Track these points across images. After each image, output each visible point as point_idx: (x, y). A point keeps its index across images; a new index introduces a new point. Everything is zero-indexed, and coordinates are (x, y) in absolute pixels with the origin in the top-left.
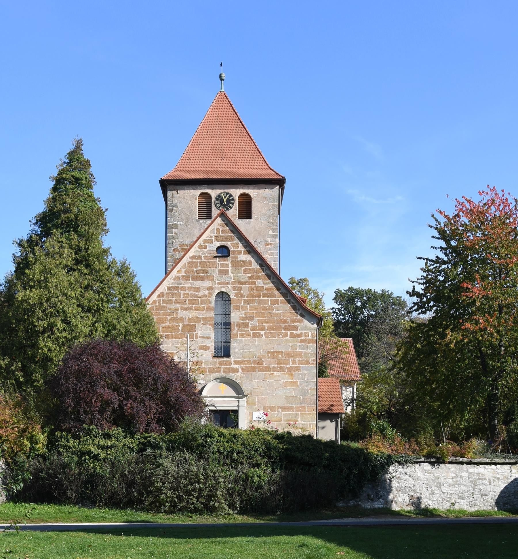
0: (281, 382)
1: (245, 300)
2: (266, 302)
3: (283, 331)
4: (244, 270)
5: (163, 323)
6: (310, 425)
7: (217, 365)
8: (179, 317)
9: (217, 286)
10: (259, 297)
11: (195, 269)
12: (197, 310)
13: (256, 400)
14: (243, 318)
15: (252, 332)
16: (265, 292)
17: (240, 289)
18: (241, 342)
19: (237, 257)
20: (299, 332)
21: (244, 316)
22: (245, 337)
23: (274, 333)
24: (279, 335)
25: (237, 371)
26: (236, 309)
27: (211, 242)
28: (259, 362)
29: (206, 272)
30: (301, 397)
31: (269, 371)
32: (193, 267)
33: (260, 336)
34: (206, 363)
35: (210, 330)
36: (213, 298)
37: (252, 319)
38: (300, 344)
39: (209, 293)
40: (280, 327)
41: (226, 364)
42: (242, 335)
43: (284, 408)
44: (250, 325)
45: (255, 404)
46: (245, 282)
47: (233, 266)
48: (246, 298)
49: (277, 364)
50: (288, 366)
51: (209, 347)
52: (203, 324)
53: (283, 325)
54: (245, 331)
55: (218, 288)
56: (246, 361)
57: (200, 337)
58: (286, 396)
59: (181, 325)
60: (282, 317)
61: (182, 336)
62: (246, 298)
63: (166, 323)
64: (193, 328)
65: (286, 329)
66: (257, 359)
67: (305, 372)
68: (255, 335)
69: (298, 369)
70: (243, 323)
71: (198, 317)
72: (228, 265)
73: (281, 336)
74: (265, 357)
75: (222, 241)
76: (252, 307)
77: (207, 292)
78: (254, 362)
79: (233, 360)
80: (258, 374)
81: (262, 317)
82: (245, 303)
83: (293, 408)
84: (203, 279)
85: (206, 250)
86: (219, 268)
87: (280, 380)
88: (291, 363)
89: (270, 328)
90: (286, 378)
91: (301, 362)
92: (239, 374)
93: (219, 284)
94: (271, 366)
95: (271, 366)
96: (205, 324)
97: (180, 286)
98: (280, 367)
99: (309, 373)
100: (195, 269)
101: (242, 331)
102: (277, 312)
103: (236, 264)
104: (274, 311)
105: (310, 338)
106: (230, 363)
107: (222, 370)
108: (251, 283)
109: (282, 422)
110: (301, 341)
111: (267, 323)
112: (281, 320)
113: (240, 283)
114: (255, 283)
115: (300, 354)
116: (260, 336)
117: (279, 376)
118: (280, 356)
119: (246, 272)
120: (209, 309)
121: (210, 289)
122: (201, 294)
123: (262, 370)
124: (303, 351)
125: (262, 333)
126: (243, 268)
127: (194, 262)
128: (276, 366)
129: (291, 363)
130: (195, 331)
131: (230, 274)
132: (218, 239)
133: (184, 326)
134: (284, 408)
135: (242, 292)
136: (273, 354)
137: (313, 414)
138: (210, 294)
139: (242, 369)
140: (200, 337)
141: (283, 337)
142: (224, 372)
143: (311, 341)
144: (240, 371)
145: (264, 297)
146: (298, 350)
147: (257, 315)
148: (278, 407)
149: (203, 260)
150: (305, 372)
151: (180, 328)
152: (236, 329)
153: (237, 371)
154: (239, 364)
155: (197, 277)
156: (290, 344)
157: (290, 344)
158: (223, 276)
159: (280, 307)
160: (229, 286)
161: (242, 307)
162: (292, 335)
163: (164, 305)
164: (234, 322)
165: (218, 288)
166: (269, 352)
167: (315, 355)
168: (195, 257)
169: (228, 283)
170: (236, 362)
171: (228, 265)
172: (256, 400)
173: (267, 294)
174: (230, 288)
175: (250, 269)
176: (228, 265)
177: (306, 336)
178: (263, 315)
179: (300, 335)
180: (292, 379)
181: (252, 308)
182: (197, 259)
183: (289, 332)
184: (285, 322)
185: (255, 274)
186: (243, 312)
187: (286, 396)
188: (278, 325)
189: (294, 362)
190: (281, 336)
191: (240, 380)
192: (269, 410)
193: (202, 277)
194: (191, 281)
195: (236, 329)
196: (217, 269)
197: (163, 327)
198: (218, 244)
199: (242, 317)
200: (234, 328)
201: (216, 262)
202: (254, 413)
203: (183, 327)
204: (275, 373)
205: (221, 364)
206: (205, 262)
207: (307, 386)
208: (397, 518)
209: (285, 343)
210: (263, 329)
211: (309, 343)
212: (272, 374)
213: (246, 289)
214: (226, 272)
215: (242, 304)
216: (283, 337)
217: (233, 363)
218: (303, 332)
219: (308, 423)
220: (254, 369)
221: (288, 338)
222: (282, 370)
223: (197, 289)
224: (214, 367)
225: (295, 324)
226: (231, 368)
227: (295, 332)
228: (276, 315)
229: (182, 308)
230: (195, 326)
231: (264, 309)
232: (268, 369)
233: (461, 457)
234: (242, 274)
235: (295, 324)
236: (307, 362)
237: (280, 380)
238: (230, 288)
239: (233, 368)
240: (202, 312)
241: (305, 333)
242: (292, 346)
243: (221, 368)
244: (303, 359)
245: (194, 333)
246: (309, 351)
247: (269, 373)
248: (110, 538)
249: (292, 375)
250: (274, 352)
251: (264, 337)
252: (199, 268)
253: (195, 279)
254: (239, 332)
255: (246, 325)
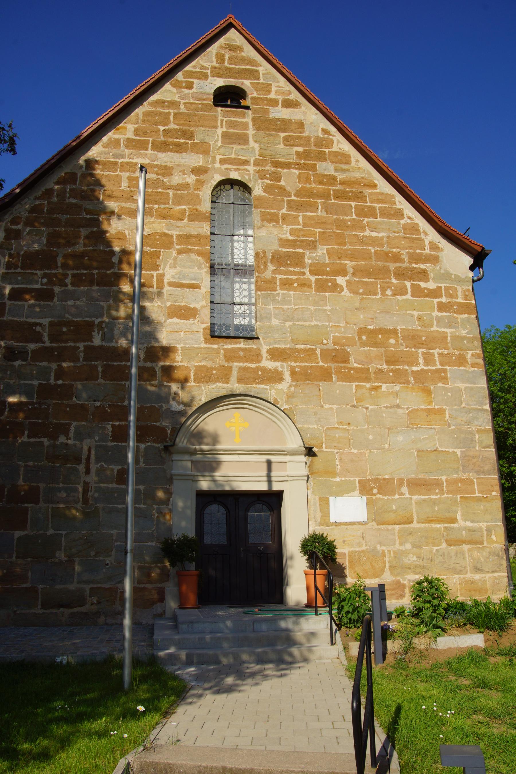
0: (400, 411)
2: (346, 211)
3: (394, 280)
4: (285, 139)
5: (69, 244)
7: (220, 361)
9: (217, 165)
11: (162, 128)
12: (165, 217)
13: (337, 462)
15: (313, 278)
16: (338, 187)
17: (277, 177)
19: (267, 111)
20: (431, 285)
21: (291, 238)
22: (295, 289)
23: (372, 283)
25: (275, 377)
26: (269, 221)
28: (339, 356)
29: (190, 135)
30: (458, 452)
31: (367, 379)
32: (157, 123)
33: (335, 288)
34: (188, 352)
35: (200, 268)
36: (206, 193)
37: (312, 246)
38: (440, 314)
39: (197, 180)
41: (246, 359)
42: (287, 284)
43: (417, 485)
44: (307, 261)
45: (334, 474)
46: (290, 163)
50: (415, 369)
51: (195, 309)
52: (179, 252)
53: (392, 266)
55: (218, 171)
57: (171, 284)
58: (419, 451)
60: (385, 248)
63: (74, 244)
65: (400, 274)
66: (331, 346)
67: (462, 386)
68: (321, 286)
69: (441, 376)
70: (288, 256)
71: (166, 235)
72: (245, 126)
73: (389, 292)
74: (350, 342)
76: (311, 218)
77: (191, 179)
78: (326, 355)
80: (338, 386)
81: (338, 244)
82: (289, 208)
84: (179, 148)
85: (191, 91)
86: (224, 129)
87: (398, 406)
90: (413, 400)
91: (446, 359)
92: (283, 386)
93: (223, 161)
94: (372, 367)
95: (372, 367)
96: (188, 251)
97: (120, 161)
98: (395, 372)
99: (471, 389)
100: (162, 128)
103: (265, 124)
104: (367, 233)
105: (460, 300)
106: (258, 357)
107: (235, 373)
108: (305, 167)
109: (415, 525)
110: (442, 307)
111: (352, 258)
112: (387, 254)
113: (276, 164)
114: (313, 167)
115: (440, 340)
116: (335, 288)
117: (396, 394)
118: (392, 341)
120: (196, 216)
121: (198, 171)
122: (176, 179)
123: (347, 378)
124: (448, 330)
125: (341, 280)
126: (282, 135)
127: (161, 113)
128: (385, 366)
129: (421, 361)
131: (252, 143)
132: (217, 73)
134: (417, 485)
135: (282, 183)
136: (374, 337)
138: (200, 183)
139: (293, 373)
140: (171, 284)
141: (394, 295)
142: (240, 380)
143: (463, 308)
144: (287, 376)
145: (336, 197)
146: (435, 328)
147: (324, 238)
150: (462, 386)
152: (271, 267)
154: (284, 360)
155: (165, 143)
156: (416, 313)
157: (416, 313)
158: (235, 147)
159: (381, 223)
160: (251, 168)
161: (284, 217)
162: (417, 292)
163: (74, 201)
165: (218, 171)
166: (362, 331)
167: (477, 343)
168: (164, 102)
169: (246, 162)
170: (276, 354)
171: (245, 126)
172: (337, 462)
175: (301, 138)
176: (247, 124)
178: (340, 240)
179: (435, 293)
182: (169, 107)
183: (408, 284)
184: (397, 258)
186: (287, 228)
187: (419, 451)
188: (380, 264)
189: (428, 359)
190: (389, 292)
191: (287, 402)
192: (375, 491)
193: (178, 145)
194: (150, 152)
198: (220, 82)
199: (288, 240)
200: (266, 266)
204: (384, 387)
205: (230, 356)
206: (189, 115)
207: (469, 423)
209: (401, 312)
210: (343, 272)
211: (459, 312)
213: (290, 179)
214: (243, 139)
215: (284, 211)
216: (394, 295)
217: (264, 354)
218: (443, 286)
219: (484, 525)
220: (326, 375)
221: (409, 296)
222: (399, 377)
223: (167, 171)
224: (209, 364)
225: (422, 266)
227: (423, 285)
228: (373, 241)
230: (157, 255)
231: (340, 224)
232: (362, 375)
233: (69, 247)
234: (282, 146)
235: (422, 266)
236: (461, 361)
237: (398, 406)
238: (252, 172)
239: (264, 370)
240: (179, 224)
241: (447, 289)
242: (419, 319)
243: (231, 368)
244: (451, 351)
245: (155, 273)
247: (368, 385)
248: (252, 394)
249: (427, 392)
251: (346, 292)
252: (172, 126)
253: (161, 147)
254: (279, 277)
255: (298, 260)
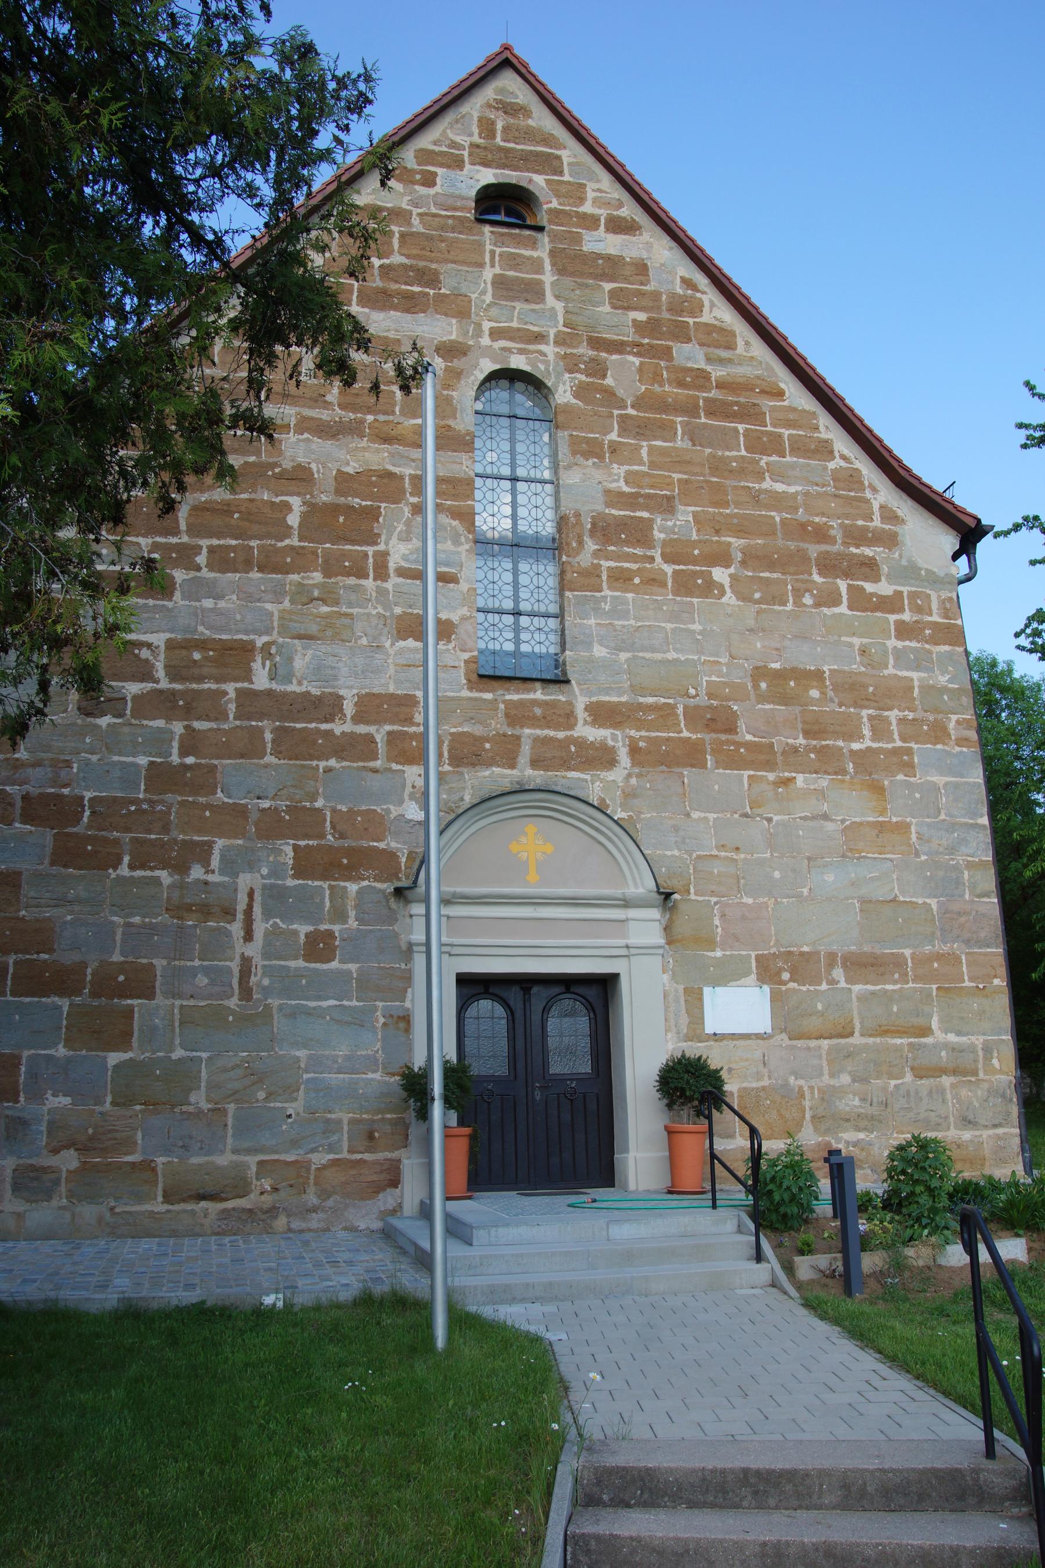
0: (830, 826)
1: (623, 419)
2: (728, 439)
3: (817, 578)
4: (613, 293)
6: (987, 1049)
7: (498, 725)
8: (287, 465)
9: (486, 341)
10: (692, 410)
12: (387, 440)
13: (717, 921)
14: (614, 498)
15: (669, 569)
16: (713, 394)
17: (598, 370)
18: (618, 611)
19: (577, 239)
20: (884, 588)
21: (626, 489)
22: (636, 590)
23: (777, 581)
24: (798, 594)
25: (604, 758)
26: (587, 455)
27: (457, 164)
28: (718, 720)
29: (431, 279)
30: (933, 903)
31: (770, 765)
33: (710, 588)
35: (456, 542)
37: (667, 506)
38: (900, 644)
40: (805, 559)
41: (545, 722)
42: (620, 579)
43: (861, 965)
44: (658, 535)
45: (710, 943)
46: (623, 343)
47: (561, 270)
48: (631, 411)
49: (807, 734)
50: (856, 746)
53: (814, 550)
54: (634, 558)
55: (487, 352)
56: (651, 708)
57: (402, 572)
58: (864, 901)
59: (295, 501)
61: (301, 561)
62: (631, 411)
64: (362, 525)
65: (829, 566)
66: (703, 700)
67: (940, 780)
68: (685, 585)
70: (622, 524)
71: (391, 475)
72: (537, 266)
75: (504, 166)
78: (693, 716)
79: (581, 703)
80: (717, 778)
82: (623, 431)
83: (898, 962)
84: (411, 304)
85: (432, 191)
86: (497, 270)
87: (825, 817)
88: (866, 732)
89: (749, 558)
90: (853, 806)
92: (616, 775)
93: (496, 334)
99: (956, 786)
101: (618, 557)
102: (780, 487)
103: (574, 264)
104: (767, 484)
105: (936, 618)
106: (568, 719)
109: (857, 1040)
110: (904, 631)
111: (740, 531)
112: (803, 526)
113: (596, 343)
114: (666, 353)
117: (821, 794)
118: (815, 693)
119: (620, 301)
123: (732, 761)
124: (915, 675)
125: (720, 575)
126: (608, 286)
128: (801, 741)
129: (866, 732)
130: (372, 539)
131: (550, 301)
132: (484, 157)
133: (312, 510)
134: (861, 965)
135: (609, 381)
136: (783, 684)
137: (997, 990)
139: (634, 751)
140: (402, 572)
141: (817, 605)
142: (535, 763)
144: (624, 759)
145: (710, 414)
146: (890, 670)
147: (689, 492)
148: (832, 957)
149: (417, 225)
150: (940, 780)
151: (293, 520)
153: (604, 758)
154: (616, 725)
155: (384, 292)
157: (857, 641)
158: (519, 306)
159: (793, 466)
160: (550, 349)
161: (614, 448)
164: (578, 515)
165: (487, 352)
167: (967, 701)
169: (539, 338)
170: (602, 714)
171: (537, 266)
172: (717, 921)
173: (725, 403)
174: (551, 357)
175: (641, 294)
177: (918, 610)
178: (718, 496)
179: (890, 604)
180: (883, 812)
181: (662, 460)
183: (843, 585)
184: (821, 535)
185: (666, 315)
186: (619, 470)
187: (864, 901)
188: (792, 545)
189: (880, 730)
190: (808, 600)
191: (624, 807)
192: (786, 976)
193: (410, 297)
195: (590, 545)
196: (488, 274)
197: (196, 509)
198: (488, 176)
199: (622, 494)
200: (581, 543)
201: (481, 245)
202: (707, 991)
203: (305, 517)
206: (429, 238)
207: (952, 850)
208: (517, 692)
210: (722, 558)
211: (935, 641)
212: (787, 782)
213: (624, 374)
214: (533, 292)
215: (613, 436)
216: (817, 605)
217: (581, 714)
218: (905, 589)
219: (978, 1040)
220: (691, 755)
221: (843, 609)
222: (827, 761)
224: (478, 730)
225: (868, 552)
226: (570, 740)
227: (869, 587)
228: (778, 501)
229: (304, 425)
230: (373, 514)
231: (718, 466)
232: (761, 756)
234: (607, 308)
235: (868, 552)
237: (825, 817)
238: (551, 357)
239: (581, 743)
241: (913, 596)
242: (863, 652)
243: (518, 738)
244: (920, 714)
245: (370, 550)
246: (943, 680)
247: (771, 776)
249: (878, 790)
250: (779, 676)
251: (729, 598)
254: (606, 564)
255: (640, 533)
